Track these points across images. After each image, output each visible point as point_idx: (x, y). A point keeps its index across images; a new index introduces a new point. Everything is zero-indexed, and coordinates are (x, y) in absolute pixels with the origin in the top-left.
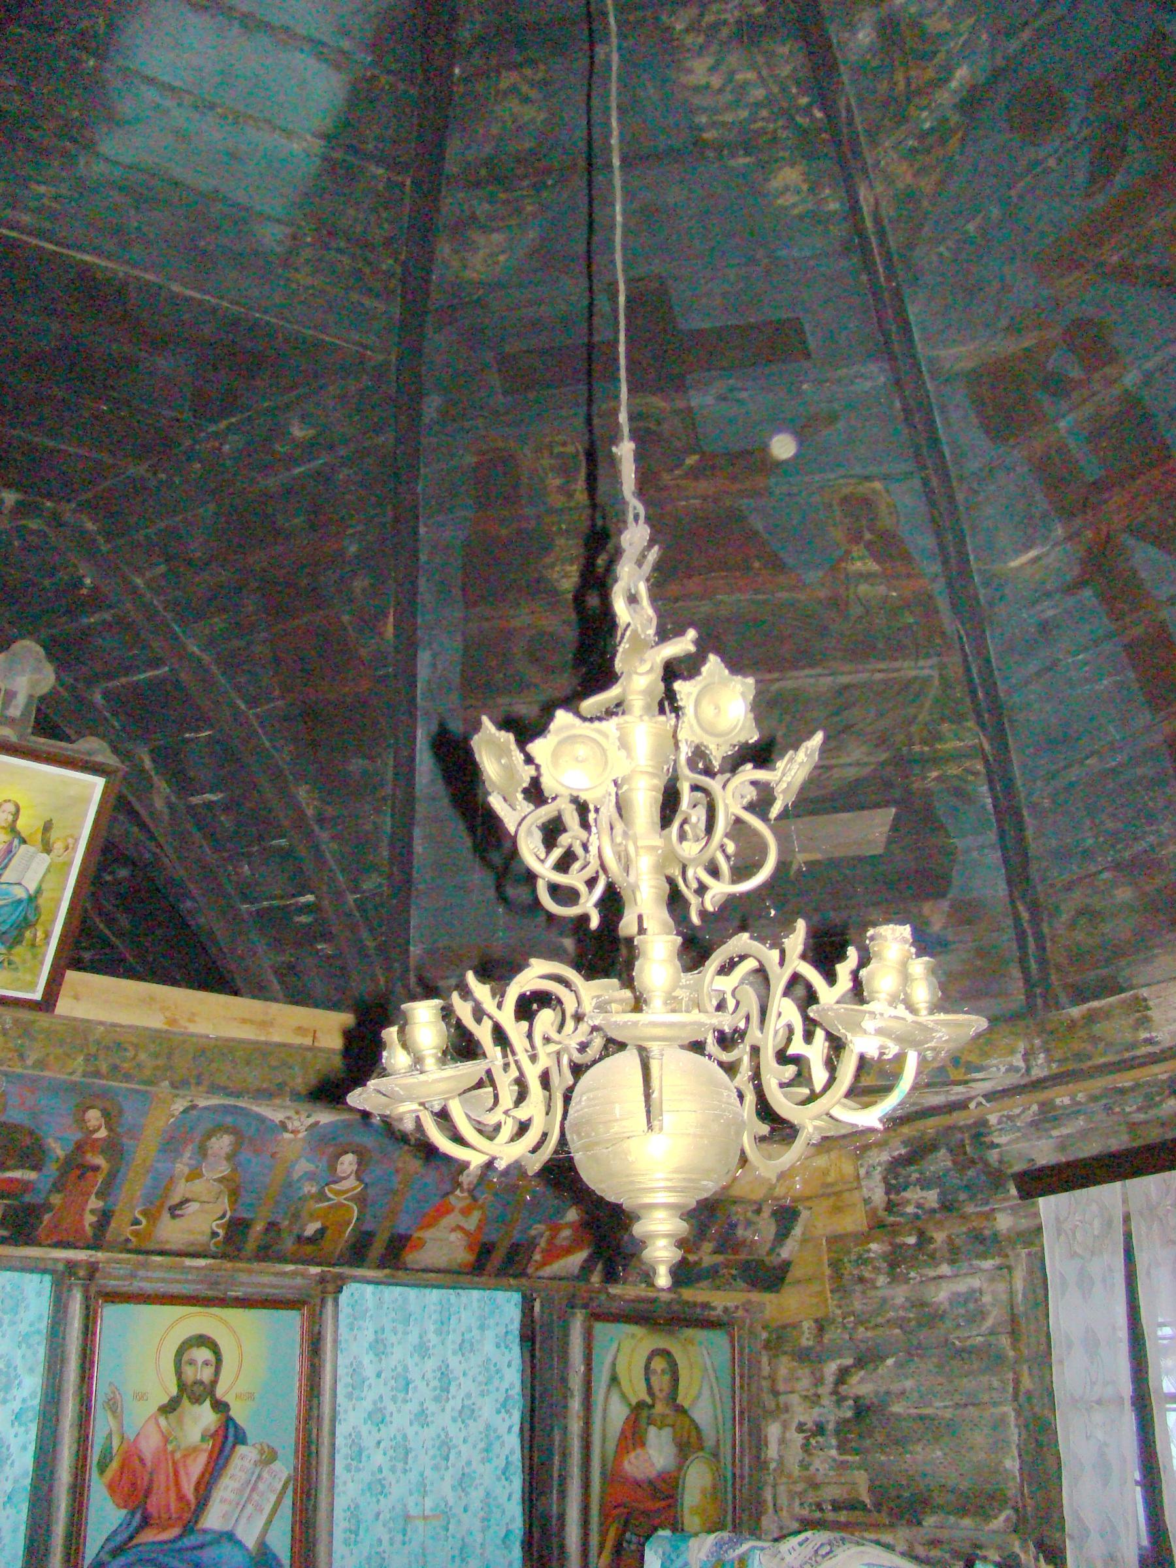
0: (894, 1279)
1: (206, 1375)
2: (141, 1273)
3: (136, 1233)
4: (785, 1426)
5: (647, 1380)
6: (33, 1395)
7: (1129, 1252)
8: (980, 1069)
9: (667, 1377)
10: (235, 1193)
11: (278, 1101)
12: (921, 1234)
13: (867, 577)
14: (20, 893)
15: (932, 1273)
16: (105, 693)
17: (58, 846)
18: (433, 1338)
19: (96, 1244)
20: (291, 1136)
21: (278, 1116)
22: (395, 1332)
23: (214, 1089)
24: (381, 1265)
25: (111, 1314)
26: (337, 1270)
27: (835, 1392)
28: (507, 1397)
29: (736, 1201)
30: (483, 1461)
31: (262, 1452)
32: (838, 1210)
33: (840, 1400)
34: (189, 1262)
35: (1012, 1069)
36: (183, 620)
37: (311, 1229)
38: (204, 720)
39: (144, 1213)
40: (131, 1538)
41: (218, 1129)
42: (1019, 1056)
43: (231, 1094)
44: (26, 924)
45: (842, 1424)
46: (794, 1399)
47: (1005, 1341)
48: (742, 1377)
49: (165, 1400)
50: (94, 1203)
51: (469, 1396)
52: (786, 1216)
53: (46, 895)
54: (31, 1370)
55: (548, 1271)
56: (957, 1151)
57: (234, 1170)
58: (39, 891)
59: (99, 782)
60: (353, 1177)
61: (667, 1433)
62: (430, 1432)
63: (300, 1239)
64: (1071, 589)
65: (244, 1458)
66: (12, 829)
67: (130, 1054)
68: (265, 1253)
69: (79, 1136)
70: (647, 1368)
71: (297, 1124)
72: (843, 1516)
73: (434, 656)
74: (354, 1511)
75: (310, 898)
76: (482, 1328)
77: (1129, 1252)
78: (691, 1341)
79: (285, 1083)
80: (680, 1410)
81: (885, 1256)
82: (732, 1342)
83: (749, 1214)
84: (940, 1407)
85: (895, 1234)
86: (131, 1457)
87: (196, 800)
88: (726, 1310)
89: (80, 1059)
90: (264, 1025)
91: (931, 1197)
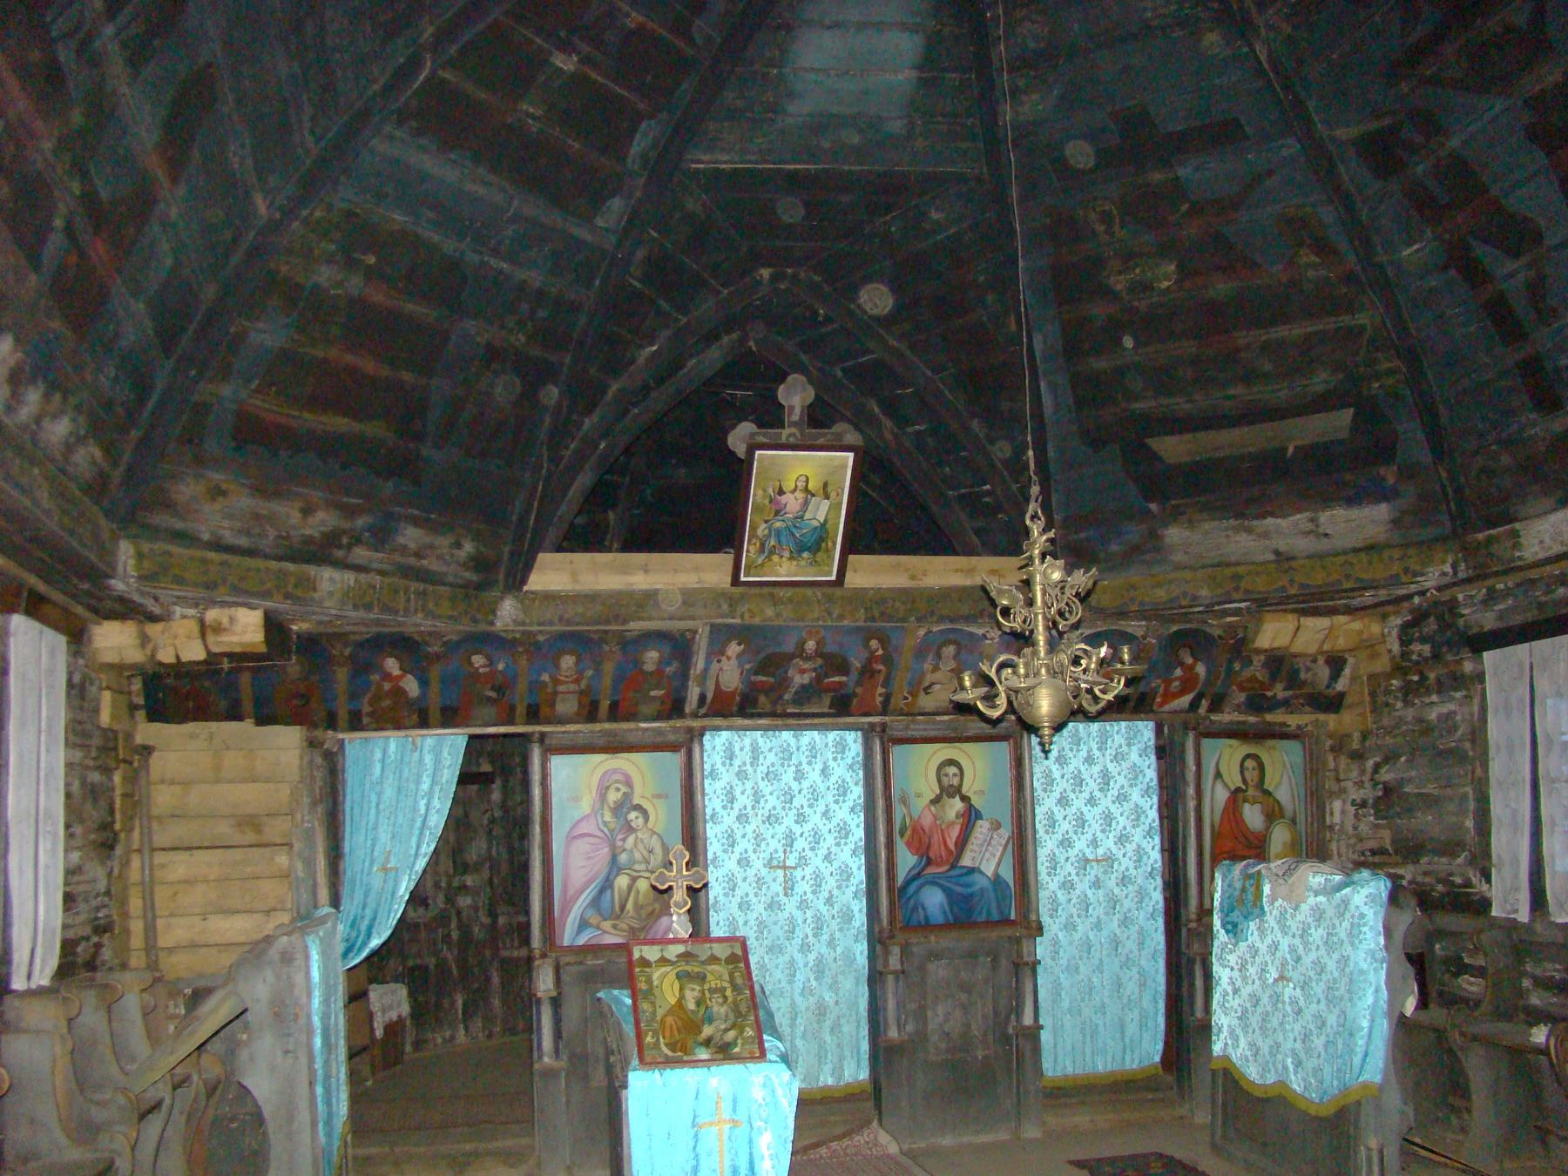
0: (1407, 703)
1: (955, 781)
2: (912, 727)
3: (906, 704)
4: (1344, 802)
5: (1242, 772)
6: (859, 797)
7: (1532, 687)
8: (1422, 575)
9: (1256, 772)
12: (1421, 673)
13: (1314, 266)
14: (815, 523)
15: (1427, 700)
16: (843, 370)
17: (833, 495)
18: (1097, 753)
19: (884, 713)
21: (980, 632)
22: (1071, 750)
23: (942, 619)
25: (897, 752)
27: (1372, 780)
29: (1295, 656)
30: (1134, 827)
31: (992, 823)
32: (1374, 656)
33: (1375, 784)
34: (938, 718)
35: (1444, 574)
39: (910, 693)
40: (923, 870)
42: (1448, 565)
43: (952, 621)
44: (821, 539)
45: (1377, 800)
47: (1467, 745)
49: (933, 796)
50: (880, 690)
51: (1122, 787)
52: (1336, 663)
54: (856, 784)
55: (1167, 708)
56: (1440, 618)
59: (851, 455)
61: (1257, 807)
62: (1097, 810)
64: (1445, 268)
65: (981, 829)
66: (806, 490)
69: (866, 655)
70: (1242, 765)
72: (1377, 859)
73: (1045, 337)
74: (1053, 859)
76: (1129, 745)
77: (1532, 687)
78: (1274, 748)
80: (1267, 793)
81: (1400, 689)
82: (1304, 749)
83: (1308, 663)
84: (1431, 789)
85: (1406, 674)
86: (917, 830)
90: (970, 571)
91: (1426, 649)
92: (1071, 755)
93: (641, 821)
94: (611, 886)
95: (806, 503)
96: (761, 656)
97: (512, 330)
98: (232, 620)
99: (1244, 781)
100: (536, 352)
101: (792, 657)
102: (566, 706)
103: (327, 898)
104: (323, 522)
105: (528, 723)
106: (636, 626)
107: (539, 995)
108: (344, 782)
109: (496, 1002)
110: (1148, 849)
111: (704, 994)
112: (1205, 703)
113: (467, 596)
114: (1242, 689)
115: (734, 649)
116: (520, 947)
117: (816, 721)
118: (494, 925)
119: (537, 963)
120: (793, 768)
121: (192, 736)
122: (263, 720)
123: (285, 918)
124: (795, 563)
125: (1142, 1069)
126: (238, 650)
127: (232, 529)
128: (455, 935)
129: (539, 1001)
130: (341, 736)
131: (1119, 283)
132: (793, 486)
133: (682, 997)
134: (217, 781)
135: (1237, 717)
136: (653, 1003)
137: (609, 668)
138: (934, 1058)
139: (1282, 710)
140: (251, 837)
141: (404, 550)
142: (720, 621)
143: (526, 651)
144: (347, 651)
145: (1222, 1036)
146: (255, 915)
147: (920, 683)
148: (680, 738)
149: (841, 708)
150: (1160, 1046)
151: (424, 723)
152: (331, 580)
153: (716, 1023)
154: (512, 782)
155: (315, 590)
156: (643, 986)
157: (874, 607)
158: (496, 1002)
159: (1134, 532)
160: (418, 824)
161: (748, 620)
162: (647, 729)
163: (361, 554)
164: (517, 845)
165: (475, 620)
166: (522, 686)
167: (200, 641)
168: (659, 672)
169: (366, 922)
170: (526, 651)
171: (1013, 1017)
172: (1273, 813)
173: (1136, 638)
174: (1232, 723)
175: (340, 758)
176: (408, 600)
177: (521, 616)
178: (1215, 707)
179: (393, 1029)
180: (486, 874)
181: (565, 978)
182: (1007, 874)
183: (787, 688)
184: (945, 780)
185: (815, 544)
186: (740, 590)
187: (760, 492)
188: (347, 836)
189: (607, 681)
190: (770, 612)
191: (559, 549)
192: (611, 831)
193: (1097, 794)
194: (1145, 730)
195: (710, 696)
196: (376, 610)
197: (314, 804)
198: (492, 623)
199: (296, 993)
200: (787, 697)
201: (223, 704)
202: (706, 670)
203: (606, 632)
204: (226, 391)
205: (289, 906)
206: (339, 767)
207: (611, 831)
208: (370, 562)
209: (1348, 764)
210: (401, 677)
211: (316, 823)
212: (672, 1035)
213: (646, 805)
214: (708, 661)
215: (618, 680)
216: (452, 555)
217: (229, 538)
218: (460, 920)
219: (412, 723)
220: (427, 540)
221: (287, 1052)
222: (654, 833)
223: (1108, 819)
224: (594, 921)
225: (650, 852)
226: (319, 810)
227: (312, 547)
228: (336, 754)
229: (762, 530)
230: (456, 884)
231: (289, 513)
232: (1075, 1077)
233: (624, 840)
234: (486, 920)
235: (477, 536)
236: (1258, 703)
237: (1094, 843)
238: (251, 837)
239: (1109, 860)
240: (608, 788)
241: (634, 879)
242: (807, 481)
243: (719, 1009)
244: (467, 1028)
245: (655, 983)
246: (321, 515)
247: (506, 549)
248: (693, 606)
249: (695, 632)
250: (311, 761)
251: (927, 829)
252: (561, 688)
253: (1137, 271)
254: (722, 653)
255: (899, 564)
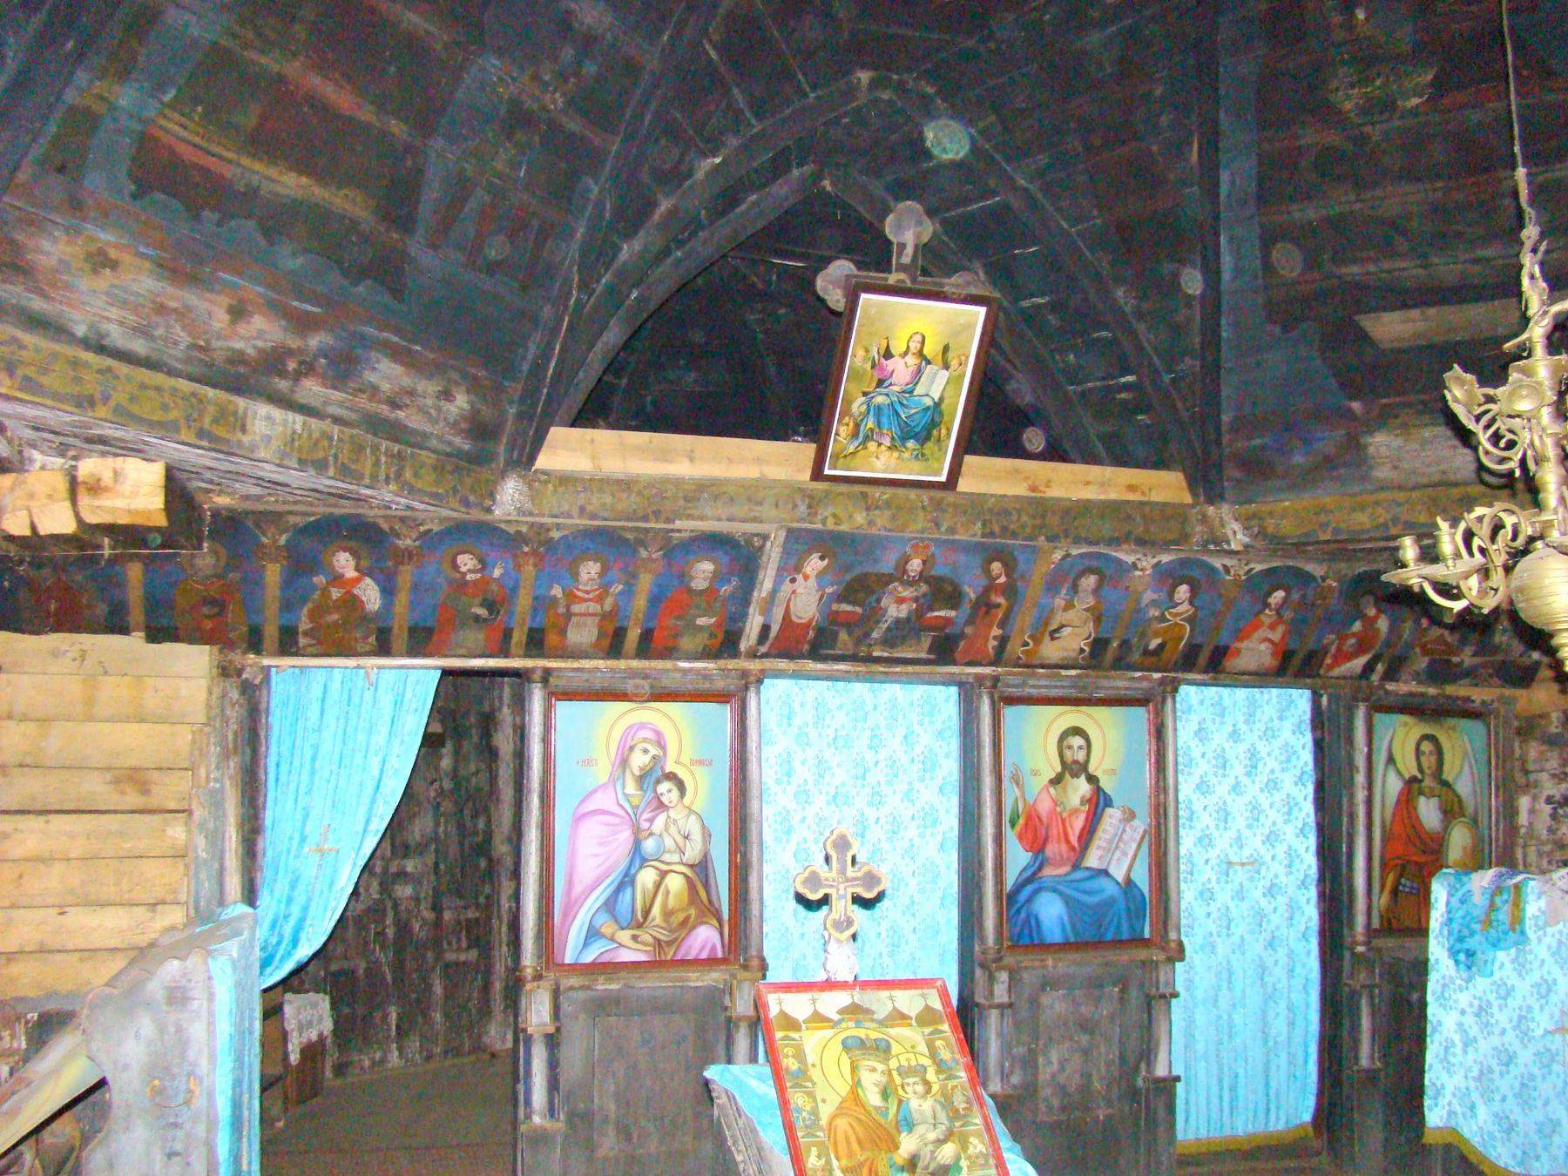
1: (1081, 756)
2: (1031, 682)
4: (1535, 798)
9: (1433, 759)
10: (1098, 620)
11: (1125, 547)
14: (928, 402)
17: (954, 363)
18: (1243, 727)
19: (996, 662)
23: (1078, 541)
24: (1206, 671)
25: (1010, 713)
26: (1172, 675)
28: (1303, 773)
30: (1286, 822)
34: (1063, 672)
36: (1009, 160)
37: (1154, 643)
38: (1029, 238)
41: (1089, 571)
43: (1091, 543)
44: (934, 424)
46: (1544, 776)
48: (1497, 757)
49: (1053, 775)
50: (996, 631)
51: (1272, 771)
53: (946, 401)
54: (947, 756)
55: (1337, 672)
57: (1098, 602)
58: (941, 399)
59: (981, 311)
61: (1434, 802)
63: (1146, 652)
65: (1111, 817)
66: (920, 354)
67: (1014, 518)
68: (1121, 663)
75: (1130, 378)
76: (1281, 718)
78: (1453, 728)
79: (1130, 532)
80: (1446, 784)
87: (1025, 304)
88: (1483, 702)
89: (979, 525)
92: (1213, 728)
93: (675, 793)
94: (633, 883)
95: (918, 372)
96: (848, 577)
97: (547, 84)
98: (117, 474)
99: (1420, 769)
100: (573, 125)
101: (886, 580)
102: (582, 634)
103: (239, 889)
104: (260, 334)
105: (527, 655)
106: (687, 526)
107: (530, 1030)
108: (268, 727)
109: (438, 1017)
110: (1302, 851)
111: (890, 1075)
112: (1380, 667)
113: (457, 469)
114: (1425, 651)
115: (814, 564)
116: (469, 947)
117: (910, 669)
118: (438, 923)
119: (528, 986)
120: (868, 733)
121: (56, 654)
122: (156, 634)
123: (176, 916)
124: (896, 454)
125: (1289, 1131)
126: (123, 520)
127: (121, 324)
128: (390, 932)
129: (529, 1040)
130: (266, 662)
131: (1348, 101)
132: (904, 349)
133: (856, 1084)
134: (91, 718)
135: (1414, 687)
136: (811, 1095)
137: (646, 582)
138: (1046, 1119)
139: (1467, 681)
140: (133, 799)
141: (374, 391)
142: (795, 525)
143: (534, 553)
144: (283, 540)
145: (1443, 1101)
146: (135, 909)
147: (1047, 623)
148: (732, 684)
149: (945, 650)
150: (1310, 1102)
151: (384, 648)
152: (268, 418)
153: (920, 1129)
154: (467, 746)
155: (243, 430)
156: (790, 1063)
157: (994, 519)
158: (438, 1017)
159: (1329, 440)
160: (369, 790)
161: (830, 525)
162: (690, 670)
163: (312, 390)
164: (469, 824)
165: (466, 503)
166: (523, 602)
167: (67, 504)
168: (711, 593)
169: (292, 922)
170: (534, 553)
171: (1143, 1066)
172: (1452, 810)
173: (1313, 578)
174: (1411, 694)
175: (264, 692)
176: (377, 463)
177: (529, 506)
178: (1391, 674)
179: (312, 1052)
180: (430, 859)
181: (566, 1007)
182: (1142, 878)
183: (878, 622)
184: (1068, 755)
185: (923, 431)
186: (821, 486)
187: (861, 353)
188: (270, 804)
189: (641, 602)
190: (860, 518)
191: (573, 424)
192: (635, 808)
193: (1244, 780)
194: (1299, 701)
195: (775, 628)
196: (331, 472)
197: (225, 755)
198: (489, 510)
199: (192, 1054)
200: (875, 635)
201: (102, 609)
202: (774, 592)
203: (647, 530)
204: (126, 97)
205: (183, 897)
206: (263, 706)
207: (635, 808)
208: (325, 403)
209: (1542, 753)
210: (357, 580)
211: (228, 783)
212: (850, 1154)
213: (682, 774)
214: (778, 583)
215: (655, 600)
216: (439, 410)
217: (117, 336)
218: (396, 914)
219: (367, 648)
220: (407, 381)
221: (171, 1155)
222: (691, 811)
223: (1255, 810)
224: (607, 930)
225: (686, 837)
226: (232, 764)
227: (242, 370)
228: (258, 687)
229: (858, 406)
230: (394, 868)
231: (212, 310)
232: (1209, 1141)
233: (651, 820)
234: (429, 915)
235: (474, 385)
236: (1441, 671)
237: (1239, 842)
238: (133, 799)
239: (1254, 863)
240: (632, 748)
241: (663, 874)
242: (923, 343)
243: (921, 1106)
244: (400, 1049)
245: (810, 1060)
246: (259, 322)
247: (512, 411)
248: (761, 504)
249: (765, 537)
250: (224, 696)
251: (1044, 819)
252: (576, 608)
253: (1378, 83)
254: (798, 569)
255: (1017, 471)
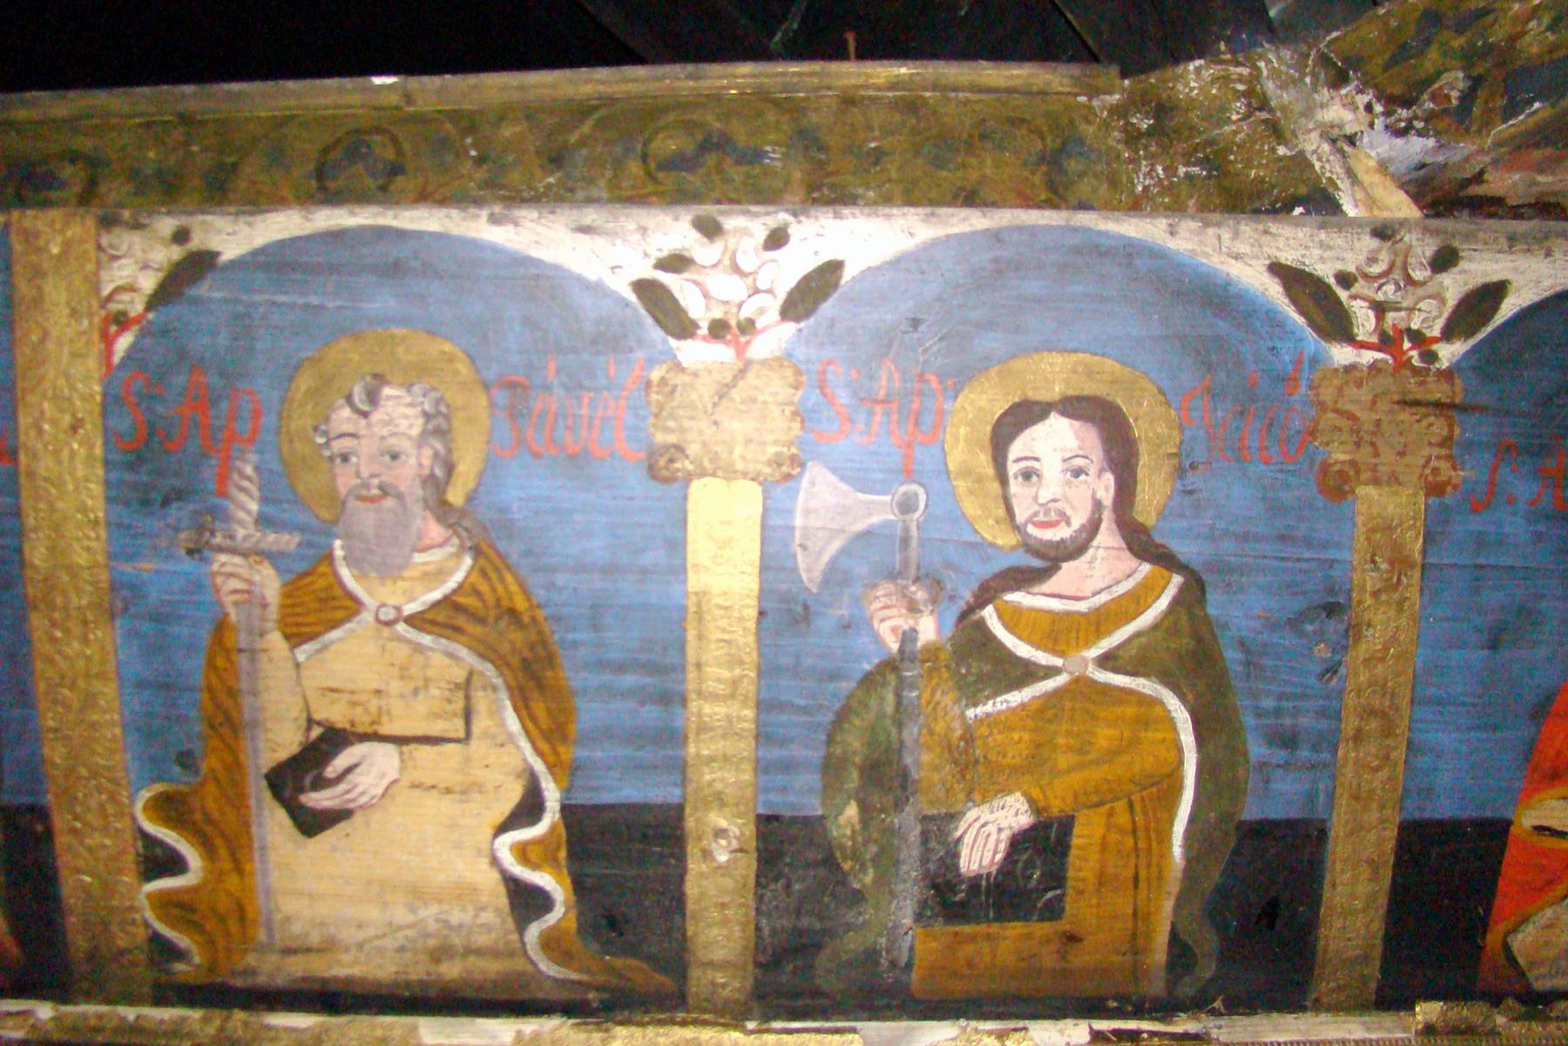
3: (177, 907)
20: (721, 353)
39: (171, 808)
60: (1107, 537)
71: (728, 288)
